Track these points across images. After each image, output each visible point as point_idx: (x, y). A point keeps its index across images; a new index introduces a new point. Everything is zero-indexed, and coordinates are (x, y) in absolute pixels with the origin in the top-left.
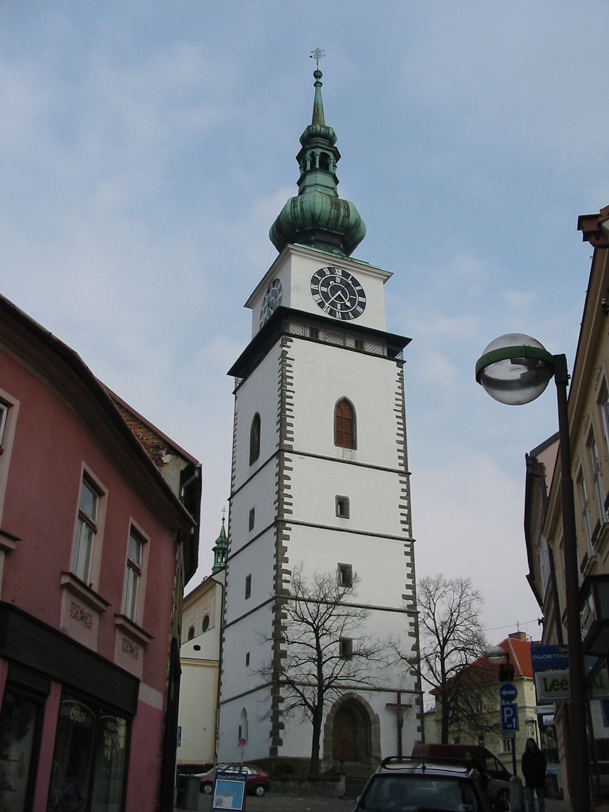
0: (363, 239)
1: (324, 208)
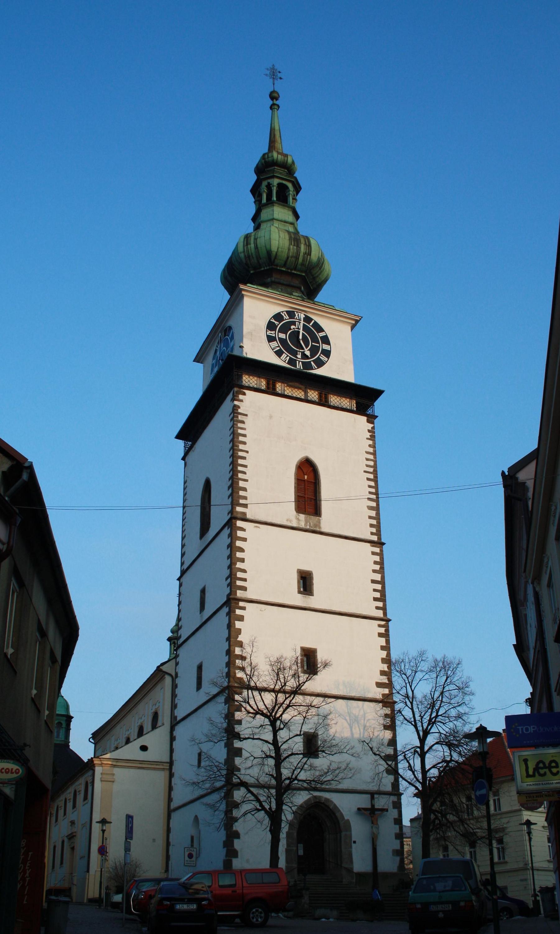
0: (327, 280)
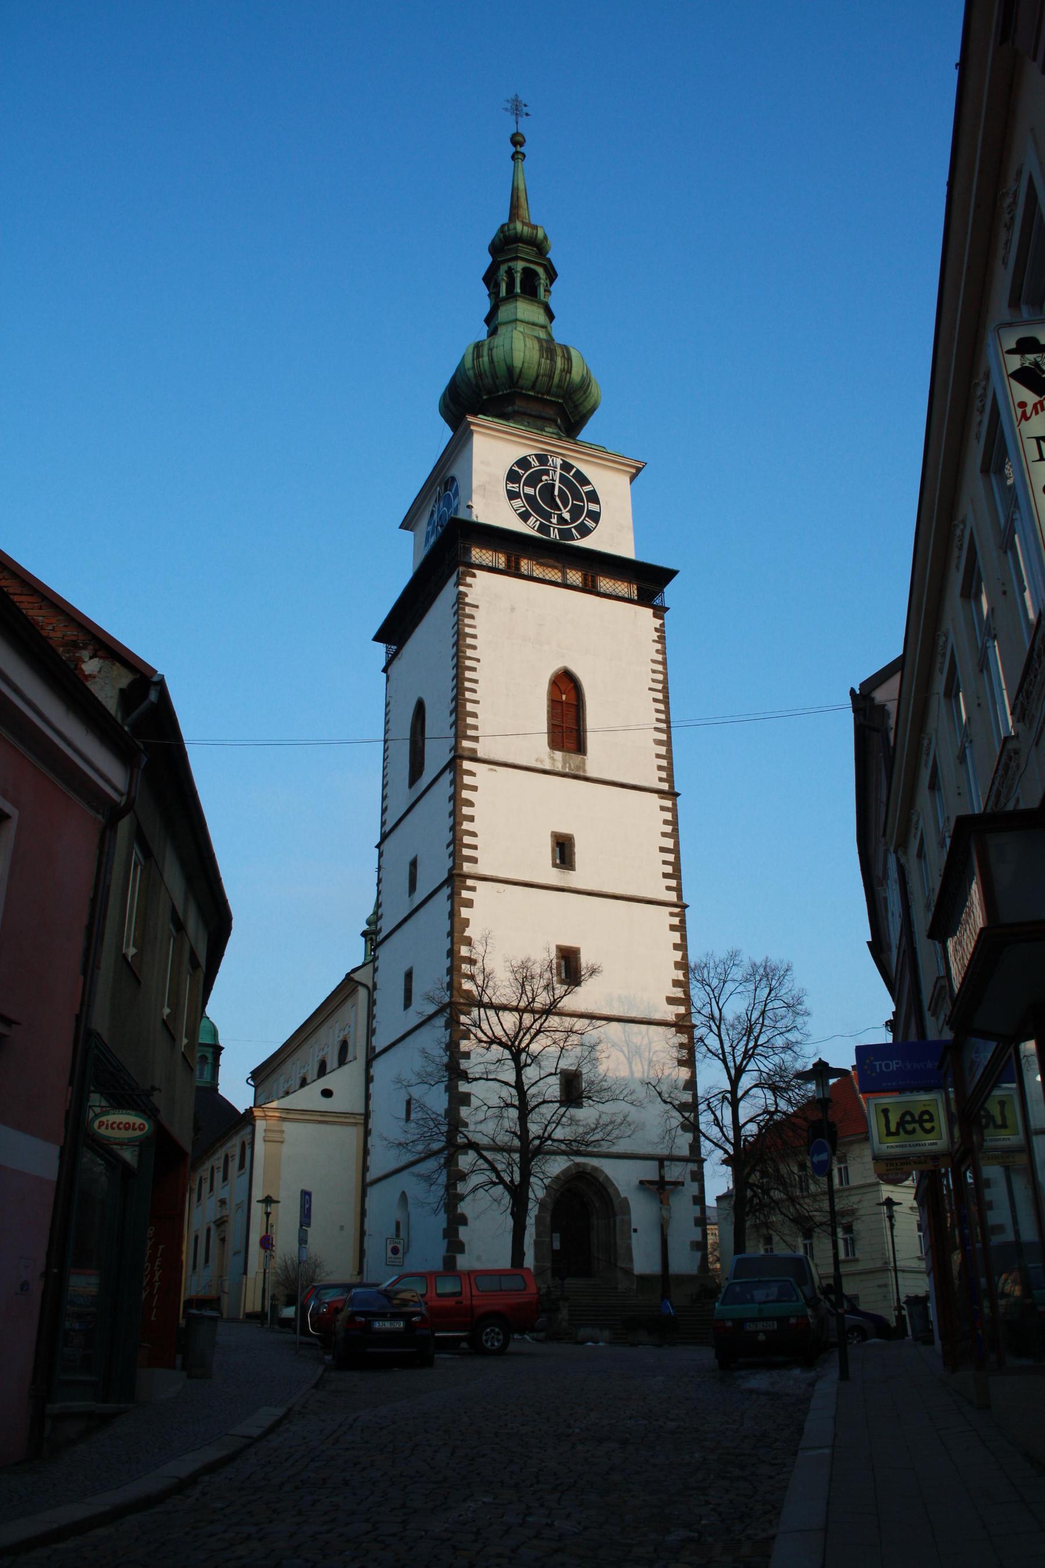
1: (528, 358)
